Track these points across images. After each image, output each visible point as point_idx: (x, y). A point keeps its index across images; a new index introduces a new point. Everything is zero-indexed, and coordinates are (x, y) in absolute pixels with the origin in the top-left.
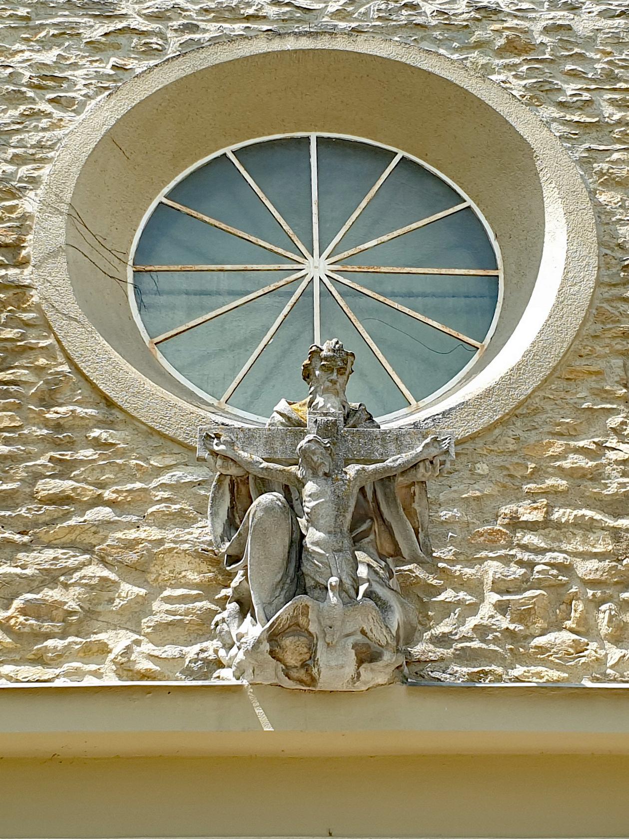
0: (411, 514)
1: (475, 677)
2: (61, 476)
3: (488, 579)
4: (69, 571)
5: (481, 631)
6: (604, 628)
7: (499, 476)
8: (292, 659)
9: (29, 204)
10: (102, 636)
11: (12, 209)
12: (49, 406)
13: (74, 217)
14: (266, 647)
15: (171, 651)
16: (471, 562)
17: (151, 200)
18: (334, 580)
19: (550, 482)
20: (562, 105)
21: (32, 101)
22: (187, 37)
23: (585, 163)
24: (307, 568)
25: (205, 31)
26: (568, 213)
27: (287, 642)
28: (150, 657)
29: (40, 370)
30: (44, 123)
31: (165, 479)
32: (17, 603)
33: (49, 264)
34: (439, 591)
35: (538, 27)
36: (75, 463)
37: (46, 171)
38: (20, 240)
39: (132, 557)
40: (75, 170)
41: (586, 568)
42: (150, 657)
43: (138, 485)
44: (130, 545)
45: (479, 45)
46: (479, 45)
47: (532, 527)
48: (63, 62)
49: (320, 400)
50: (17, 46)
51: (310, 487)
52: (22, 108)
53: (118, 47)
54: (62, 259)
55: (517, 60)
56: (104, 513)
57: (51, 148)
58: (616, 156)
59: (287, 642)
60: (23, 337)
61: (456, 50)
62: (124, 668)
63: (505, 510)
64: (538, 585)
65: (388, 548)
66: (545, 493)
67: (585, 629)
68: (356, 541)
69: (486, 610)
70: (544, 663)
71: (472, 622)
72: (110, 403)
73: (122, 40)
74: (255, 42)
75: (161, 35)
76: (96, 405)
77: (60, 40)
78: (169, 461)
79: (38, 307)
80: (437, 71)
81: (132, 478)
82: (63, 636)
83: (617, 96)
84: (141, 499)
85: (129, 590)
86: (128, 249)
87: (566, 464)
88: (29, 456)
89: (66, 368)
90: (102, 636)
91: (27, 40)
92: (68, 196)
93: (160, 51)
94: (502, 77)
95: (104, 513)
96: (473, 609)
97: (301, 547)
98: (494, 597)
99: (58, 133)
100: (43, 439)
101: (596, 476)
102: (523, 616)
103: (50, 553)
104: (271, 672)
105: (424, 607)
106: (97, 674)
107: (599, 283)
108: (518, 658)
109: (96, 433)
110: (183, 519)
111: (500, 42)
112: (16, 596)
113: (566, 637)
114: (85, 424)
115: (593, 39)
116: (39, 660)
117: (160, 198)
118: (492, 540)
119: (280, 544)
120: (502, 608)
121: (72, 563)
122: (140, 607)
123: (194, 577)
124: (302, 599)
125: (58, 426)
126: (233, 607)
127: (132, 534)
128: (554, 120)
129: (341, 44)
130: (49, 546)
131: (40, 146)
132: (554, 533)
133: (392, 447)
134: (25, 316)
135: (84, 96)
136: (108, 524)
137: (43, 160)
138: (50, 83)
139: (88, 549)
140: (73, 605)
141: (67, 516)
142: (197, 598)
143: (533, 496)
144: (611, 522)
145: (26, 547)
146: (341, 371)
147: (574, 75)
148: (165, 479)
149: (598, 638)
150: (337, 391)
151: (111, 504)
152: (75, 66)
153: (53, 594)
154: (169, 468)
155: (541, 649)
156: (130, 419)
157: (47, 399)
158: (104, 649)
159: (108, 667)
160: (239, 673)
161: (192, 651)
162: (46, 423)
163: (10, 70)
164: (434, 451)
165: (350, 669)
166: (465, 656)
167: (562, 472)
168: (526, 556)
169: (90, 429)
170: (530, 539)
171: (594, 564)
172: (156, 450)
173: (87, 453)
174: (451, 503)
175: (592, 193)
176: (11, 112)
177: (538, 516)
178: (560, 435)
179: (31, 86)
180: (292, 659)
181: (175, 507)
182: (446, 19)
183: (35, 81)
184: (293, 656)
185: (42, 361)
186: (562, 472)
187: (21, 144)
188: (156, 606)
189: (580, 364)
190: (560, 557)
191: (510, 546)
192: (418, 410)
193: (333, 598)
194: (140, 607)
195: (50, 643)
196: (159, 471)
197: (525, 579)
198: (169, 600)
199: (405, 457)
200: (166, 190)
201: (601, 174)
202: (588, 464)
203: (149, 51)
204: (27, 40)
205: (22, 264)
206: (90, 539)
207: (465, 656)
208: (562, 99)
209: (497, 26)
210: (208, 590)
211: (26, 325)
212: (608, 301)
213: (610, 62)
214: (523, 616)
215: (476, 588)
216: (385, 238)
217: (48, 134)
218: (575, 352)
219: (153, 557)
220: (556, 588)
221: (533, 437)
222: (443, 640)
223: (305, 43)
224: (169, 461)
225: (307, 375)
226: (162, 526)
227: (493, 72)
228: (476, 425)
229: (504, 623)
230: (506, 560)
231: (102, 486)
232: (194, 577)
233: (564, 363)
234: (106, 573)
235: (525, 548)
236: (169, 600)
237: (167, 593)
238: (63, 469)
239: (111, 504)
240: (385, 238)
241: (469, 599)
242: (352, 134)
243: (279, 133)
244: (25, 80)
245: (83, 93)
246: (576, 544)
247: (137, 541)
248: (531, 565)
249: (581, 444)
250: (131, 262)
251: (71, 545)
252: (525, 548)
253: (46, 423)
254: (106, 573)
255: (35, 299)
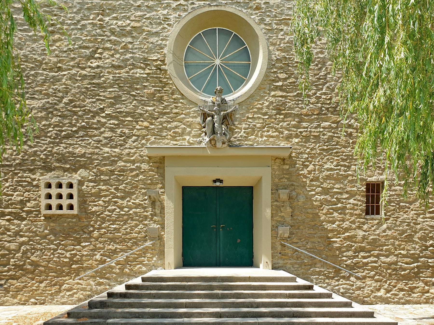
0: (231, 118)
1: (239, 144)
2: (176, 109)
3: (243, 127)
4: (179, 126)
5: (241, 136)
6: (259, 135)
7: (246, 109)
8: (213, 144)
9: (165, 51)
10: (185, 137)
11: (162, 52)
12: (173, 95)
13: (174, 54)
15: (195, 139)
16: (241, 124)
18: (219, 132)
19: (254, 110)
20: (265, 24)
21: (163, 24)
22: (193, 6)
23: (268, 39)
24: (215, 130)
25: (196, 4)
26: (263, 52)
27: (212, 141)
28: (192, 140)
29: (171, 88)
30: (166, 30)
31: (192, 110)
32: (172, 131)
33: (170, 65)
34: (235, 129)
36: (178, 107)
37: (168, 43)
38: (164, 59)
39: (188, 124)
40: (173, 43)
41: (258, 125)
42: (192, 140)
43: (188, 111)
44: (188, 122)
45: (251, 7)
46: (251, 7)
47: (250, 118)
49: (217, 98)
50: (159, 9)
51: (216, 117)
52: (162, 26)
53: (178, 9)
54: (172, 64)
55: (257, 12)
56: (183, 116)
57: (168, 37)
58: (274, 38)
59: (212, 141)
60: (167, 81)
61: (246, 9)
62: (188, 142)
63: (247, 115)
64: (250, 128)
65: (227, 124)
66: (253, 112)
67: (257, 136)
68: (222, 124)
69: (242, 133)
70: (250, 141)
71: (240, 135)
72: (183, 95)
73: (179, 7)
74: (206, 8)
75: (187, 6)
76: (180, 95)
77: (167, 7)
78: (193, 106)
79: (169, 75)
80: (241, 16)
81: (187, 109)
82: (179, 137)
83: (276, 22)
84: (189, 114)
85: (188, 129)
87: (257, 107)
88: (171, 105)
89: (175, 88)
90: (185, 137)
91: (161, 7)
92: (172, 49)
93: (187, 10)
94: (254, 17)
95: (183, 116)
96: (240, 132)
97: (214, 126)
98: (243, 131)
99: (169, 33)
100: (173, 102)
101: (262, 109)
102: (248, 134)
103: (176, 123)
104: (210, 145)
105: (233, 132)
106: (185, 143)
107: (267, 69)
108: (246, 140)
109: (181, 101)
110: (196, 117)
111: (255, 7)
112: (171, 130)
113: (254, 137)
114: (179, 99)
115: (273, 6)
116: (176, 140)
118: (244, 121)
119: (211, 126)
120: (244, 132)
121: (179, 125)
122: (190, 133)
123: (198, 127)
124: (214, 135)
125: (175, 99)
126: (204, 134)
127: (188, 120)
128: (263, 28)
129: (223, 8)
130: (176, 121)
131: (166, 36)
132: (254, 119)
133: (229, 108)
134: (167, 76)
136: (184, 118)
137: (167, 40)
138: (166, 20)
139: (181, 122)
140: (180, 132)
141: (178, 116)
142: (199, 131)
143: (251, 112)
145: (172, 122)
146: (221, 93)
147: (269, 16)
148: (192, 110)
149: (259, 137)
150: (220, 96)
151: (184, 114)
152: (171, 15)
153: (177, 130)
154: (193, 107)
155: (250, 139)
156: (186, 98)
157: (173, 94)
158: (185, 139)
159: (186, 142)
160: (205, 145)
161: (198, 139)
162: (173, 99)
163: (158, 16)
164: (235, 109)
165: (221, 145)
166: (239, 140)
167: (256, 108)
168: (249, 123)
169: (180, 100)
170: (250, 120)
171: (259, 125)
172: (191, 104)
173: (180, 105)
174: (238, 114)
175: (268, 47)
176: (160, 27)
177: (251, 116)
178: (257, 101)
179: (163, 20)
180: (213, 144)
181: (195, 115)
183: (163, 19)
184: (213, 142)
185: (171, 86)
186: (256, 108)
187: (162, 36)
188: (193, 132)
189: (262, 86)
190: (254, 123)
191: (247, 122)
192: (234, 93)
193: (219, 135)
194: (190, 133)
195: (178, 138)
196: (191, 108)
197: (248, 127)
198: (194, 131)
199: (230, 110)
200: (189, 43)
201: (271, 42)
202: (260, 106)
203: (185, 10)
204: (161, 7)
205: (165, 65)
206: (182, 120)
207: (239, 140)
208: (265, 23)
210: (200, 129)
211: (167, 78)
212: (268, 72)
213: (276, 12)
214: (247, 134)
215: (241, 129)
216: (230, 54)
217: (167, 33)
218: (261, 84)
219: (191, 124)
220: (253, 129)
221: (252, 101)
222: (235, 138)
223: (216, 8)
224: (193, 106)
225: (215, 93)
226: (193, 118)
227: (252, 15)
228: (243, 99)
229: (245, 135)
230: (246, 124)
231: (183, 111)
232: (198, 127)
233: (259, 86)
234: (185, 127)
235: (249, 122)
236: (194, 131)
237: (194, 130)
238: (176, 107)
239: (184, 114)
240: (230, 54)
241: (240, 131)
244: (161, 19)
246: (257, 121)
247: (189, 121)
248: (249, 125)
249: (260, 103)
251: (179, 122)
252: (249, 122)
253: (173, 99)
254: (185, 127)
255: (168, 73)
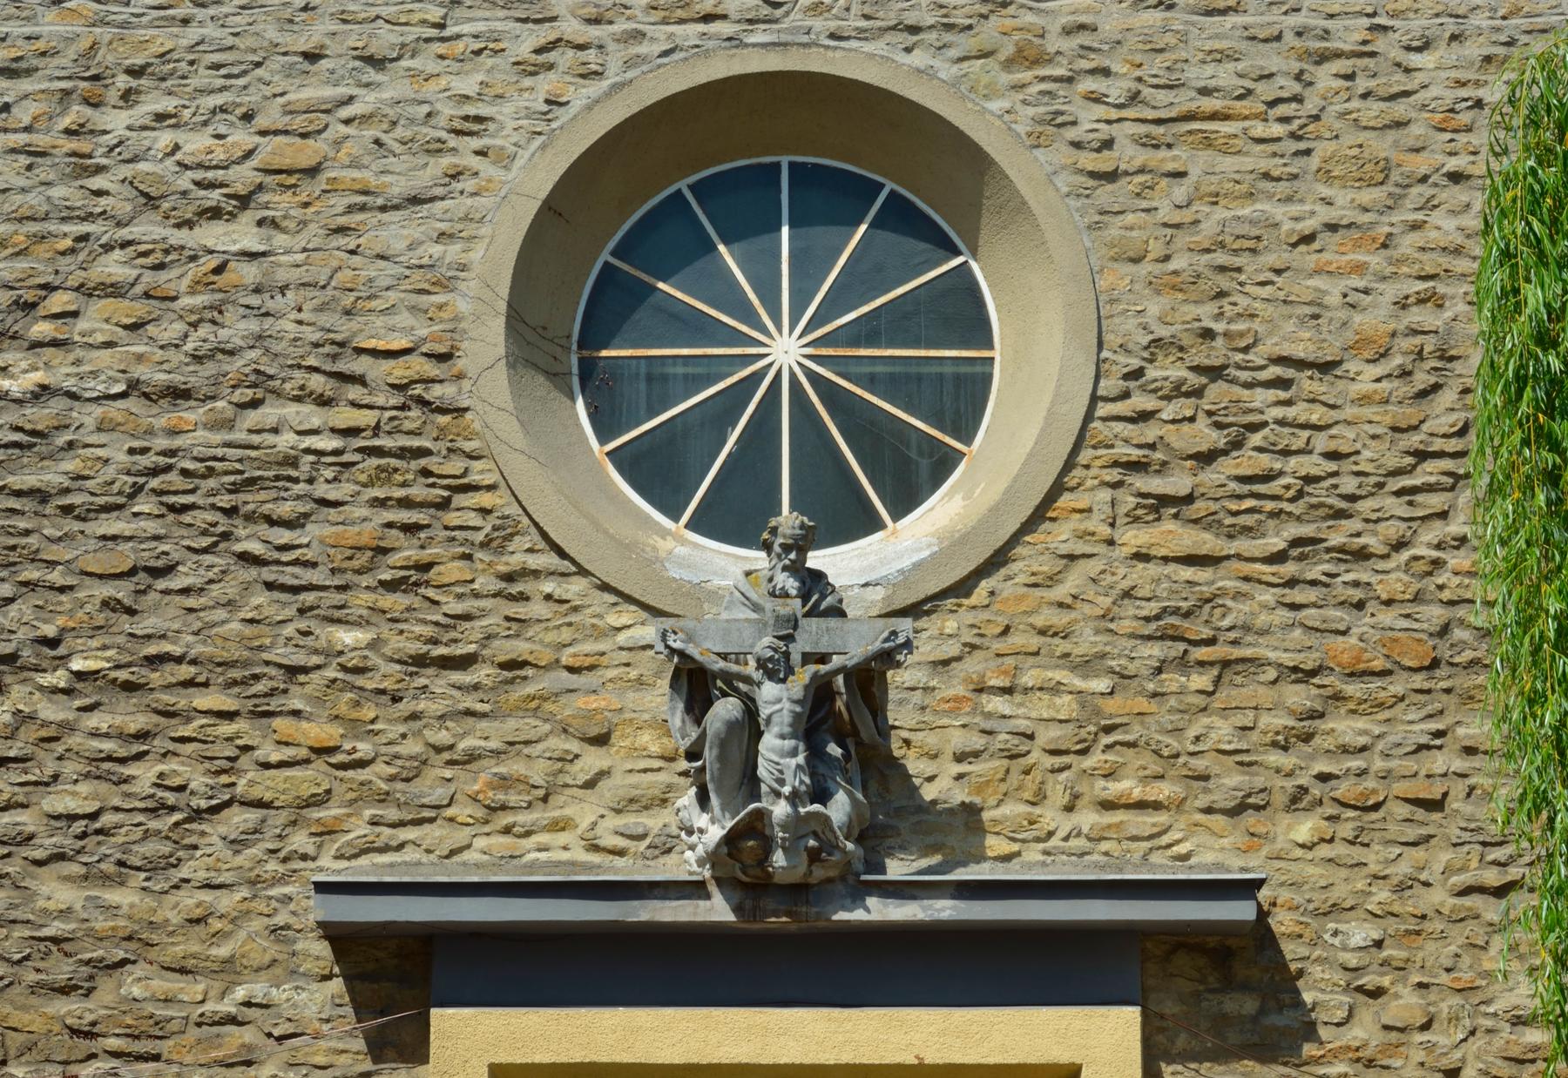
14: (725, 850)
17: (595, 260)
30: (469, 184)
35: (1055, 27)
48: (486, 91)
86: (571, 329)
90: (568, 812)
111: (1008, 50)
117: (605, 256)
135: (515, 145)
144: (1079, 683)
168: (988, 725)
182: (945, 16)
200: (611, 245)
209: (1009, 22)
242: (832, 158)
243: (743, 157)
245: (514, 140)
250: (575, 347)
